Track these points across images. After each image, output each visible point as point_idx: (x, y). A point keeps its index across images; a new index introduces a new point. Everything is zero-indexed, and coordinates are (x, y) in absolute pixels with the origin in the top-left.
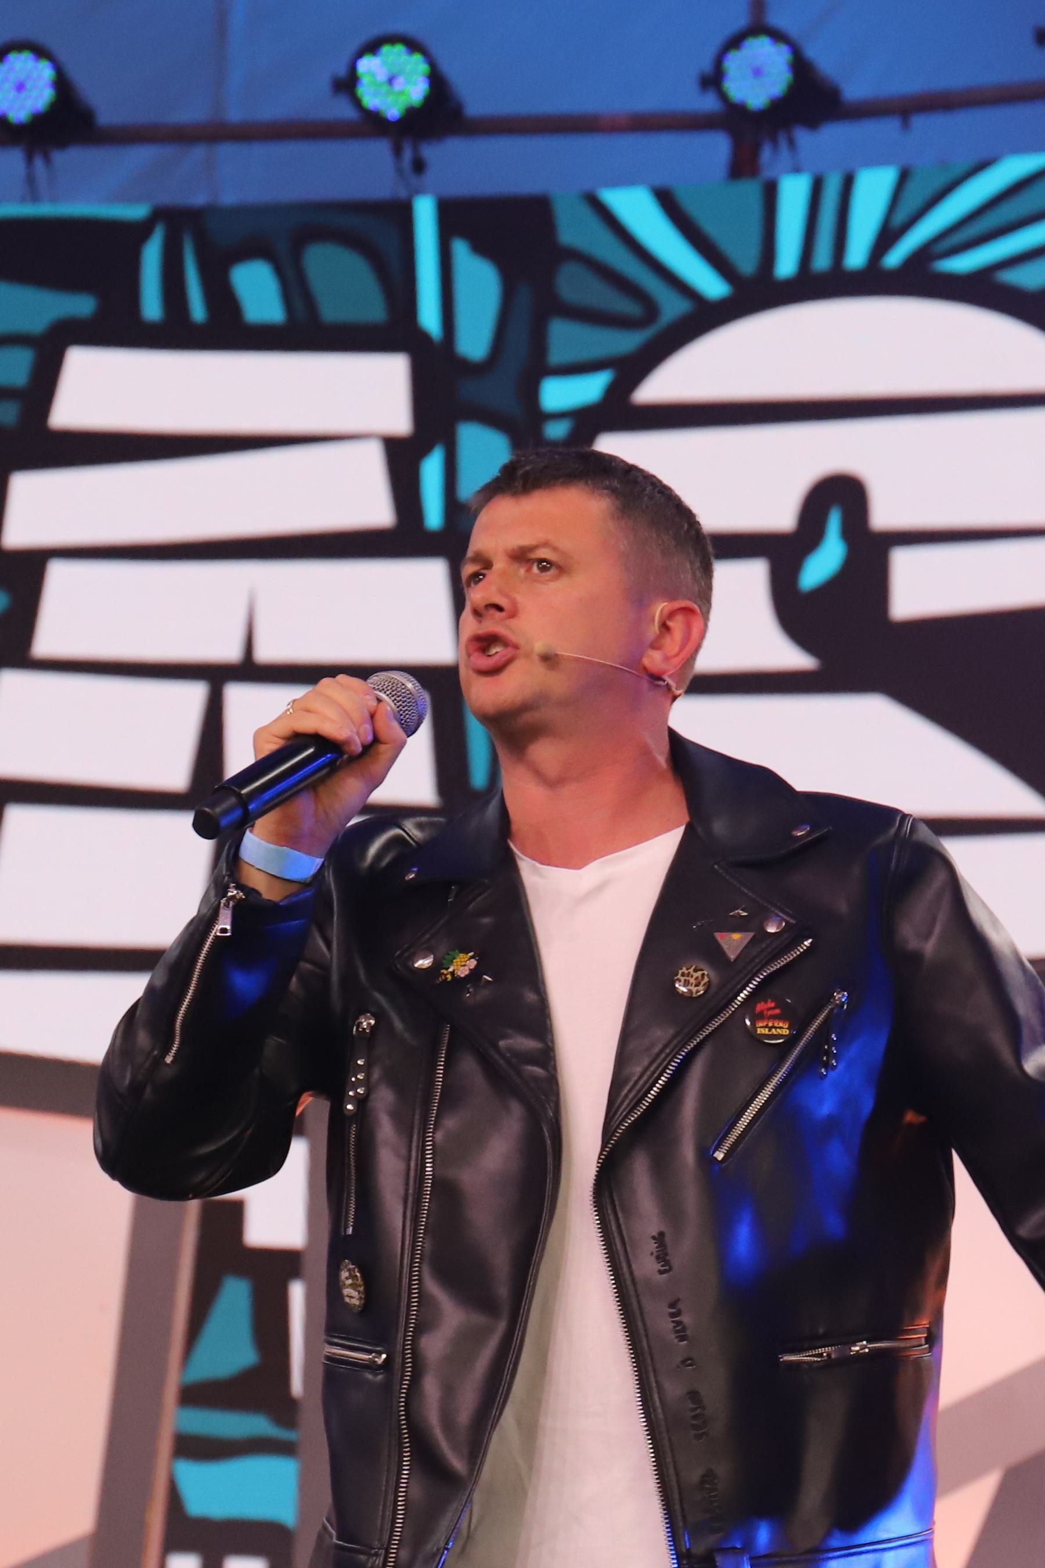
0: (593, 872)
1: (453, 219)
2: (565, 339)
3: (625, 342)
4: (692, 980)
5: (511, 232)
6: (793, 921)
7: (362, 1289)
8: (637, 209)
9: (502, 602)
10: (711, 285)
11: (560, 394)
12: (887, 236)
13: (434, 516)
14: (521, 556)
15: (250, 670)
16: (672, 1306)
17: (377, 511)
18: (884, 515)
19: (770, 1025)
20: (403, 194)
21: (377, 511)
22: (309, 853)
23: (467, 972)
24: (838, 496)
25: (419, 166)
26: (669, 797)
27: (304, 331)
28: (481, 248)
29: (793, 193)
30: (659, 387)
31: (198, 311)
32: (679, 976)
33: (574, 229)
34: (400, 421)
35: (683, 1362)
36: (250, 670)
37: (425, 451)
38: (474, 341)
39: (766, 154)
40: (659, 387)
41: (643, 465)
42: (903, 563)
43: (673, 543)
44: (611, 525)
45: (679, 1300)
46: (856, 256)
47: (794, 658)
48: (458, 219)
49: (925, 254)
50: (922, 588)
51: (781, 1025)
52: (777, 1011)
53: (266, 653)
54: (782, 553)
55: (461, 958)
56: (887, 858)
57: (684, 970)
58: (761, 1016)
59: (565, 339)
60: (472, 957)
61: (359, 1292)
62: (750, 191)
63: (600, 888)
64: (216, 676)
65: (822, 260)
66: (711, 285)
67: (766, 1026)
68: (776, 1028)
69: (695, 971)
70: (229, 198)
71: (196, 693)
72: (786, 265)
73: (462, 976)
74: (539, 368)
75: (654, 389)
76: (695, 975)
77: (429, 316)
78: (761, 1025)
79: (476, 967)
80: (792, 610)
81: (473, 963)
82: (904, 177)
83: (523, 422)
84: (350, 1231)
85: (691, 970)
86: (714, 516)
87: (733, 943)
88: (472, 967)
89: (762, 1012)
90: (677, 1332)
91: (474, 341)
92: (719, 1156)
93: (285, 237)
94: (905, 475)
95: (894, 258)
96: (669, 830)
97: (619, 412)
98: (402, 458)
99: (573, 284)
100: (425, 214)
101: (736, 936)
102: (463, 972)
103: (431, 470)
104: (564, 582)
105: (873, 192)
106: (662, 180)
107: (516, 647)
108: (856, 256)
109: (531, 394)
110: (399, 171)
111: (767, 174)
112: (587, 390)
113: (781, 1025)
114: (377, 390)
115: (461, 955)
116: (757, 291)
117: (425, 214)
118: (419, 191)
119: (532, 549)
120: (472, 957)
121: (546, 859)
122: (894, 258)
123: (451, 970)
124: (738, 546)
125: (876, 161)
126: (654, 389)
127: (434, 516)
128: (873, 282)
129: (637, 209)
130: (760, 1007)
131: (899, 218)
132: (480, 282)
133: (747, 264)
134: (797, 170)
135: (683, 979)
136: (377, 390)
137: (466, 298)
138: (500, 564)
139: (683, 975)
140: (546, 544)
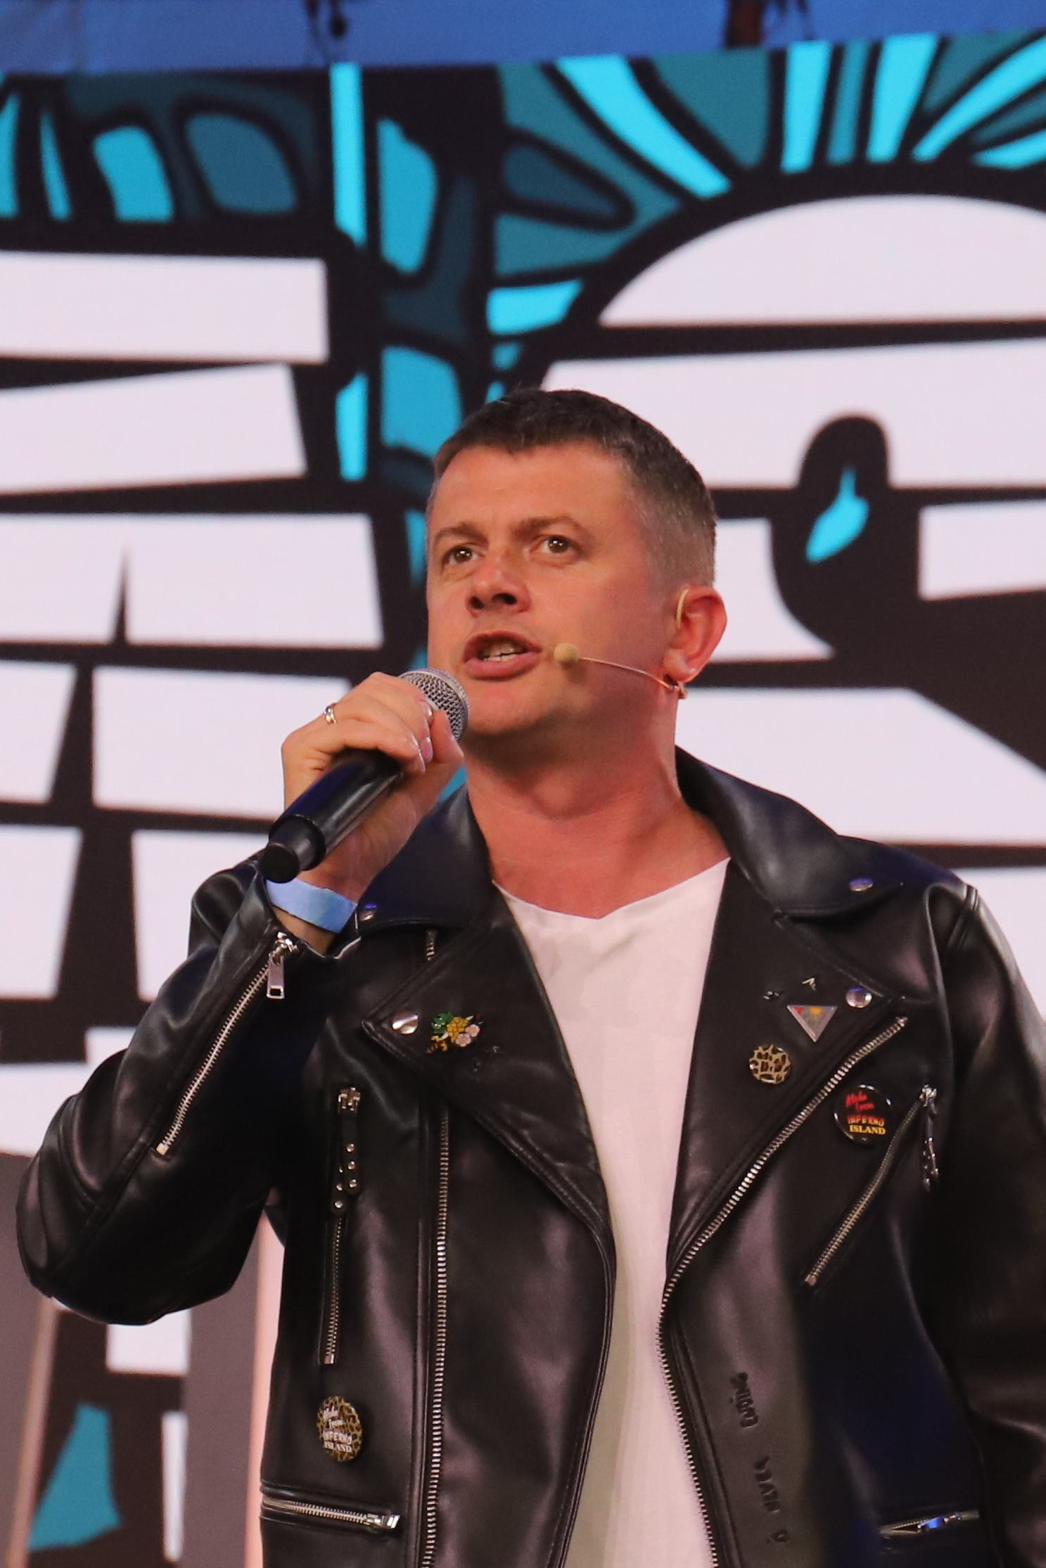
0: (619, 923)
1: (381, 94)
2: (518, 240)
3: (596, 247)
4: (771, 1064)
5: (446, 108)
6: (880, 995)
7: (359, 1433)
8: (607, 84)
9: (510, 588)
10: (704, 180)
11: (517, 311)
12: (921, 121)
13: (353, 463)
14: (529, 532)
15: (123, 652)
16: (760, 1465)
17: (282, 455)
18: (908, 467)
19: (864, 1121)
20: (318, 62)
21: (282, 455)
22: (349, 898)
23: (469, 1041)
24: (851, 448)
25: (339, 27)
26: (689, 830)
27: (202, 228)
28: (413, 134)
29: (807, 68)
30: (635, 305)
31: (59, 204)
32: (755, 1058)
33: (527, 106)
34: (311, 343)
35: (775, 1537)
36: (123, 652)
37: (344, 382)
38: (405, 246)
39: (771, 18)
40: (635, 305)
41: (615, 398)
42: (940, 531)
43: (691, 512)
44: (631, 494)
45: (767, 1459)
46: (883, 145)
47: (796, 642)
48: (386, 95)
49: (965, 144)
50: (961, 558)
51: (876, 1122)
52: (871, 1106)
53: (142, 630)
54: (787, 512)
55: (456, 1024)
56: (901, 901)
57: (761, 1049)
58: (852, 1111)
59: (518, 240)
60: (472, 1022)
61: (355, 1437)
62: (753, 62)
63: (624, 945)
64: (84, 659)
65: (841, 150)
66: (704, 180)
67: (860, 1123)
68: (871, 1126)
69: (775, 1051)
70: (97, 65)
71: (56, 682)
72: (797, 155)
73: (463, 1045)
74: (485, 279)
75: (630, 308)
76: (775, 1057)
77: (350, 214)
78: (853, 1121)
79: (479, 1034)
80: (800, 584)
81: (475, 1030)
82: (942, 48)
83: (467, 349)
84: (331, 1359)
85: (769, 1051)
86: (717, 468)
87: (812, 1020)
88: (475, 1035)
89: (853, 1106)
90: (767, 1498)
91: (405, 246)
92: (811, 1279)
93: (168, 111)
94: (937, 419)
95: (930, 147)
96: (704, 868)
97: (584, 335)
98: (314, 390)
99: (523, 174)
100: (346, 86)
101: (816, 1011)
102: (464, 1041)
103: (351, 406)
104: (581, 566)
105: (905, 65)
106: (641, 48)
107: (537, 650)
108: (883, 145)
109: (477, 312)
110: (314, 32)
111: (772, 42)
112: (543, 306)
113: (876, 1122)
114: (286, 304)
115: (456, 1019)
116: (760, 187)
117: (346, 86)
118: (341, 58)
119: (545, 523)
120: (472, 1022)
121: (553, 903)
122: (930, 147)
123: (445, 1036)
124: (740, 503)
125: (910, 28)
126: (630, 308)
127: (353, 463)
128: (903, 178)
129: (607, 84)
130: (850, 1099)
131: (935, 98)
132: (411, 175)
133: (748, 151)
134: (809, 37)
135: (760, 1061)
136: (286, 304)
137: (393, 193)
138: (498, 542)
139: (760, 1056)
140: (565, 519)
